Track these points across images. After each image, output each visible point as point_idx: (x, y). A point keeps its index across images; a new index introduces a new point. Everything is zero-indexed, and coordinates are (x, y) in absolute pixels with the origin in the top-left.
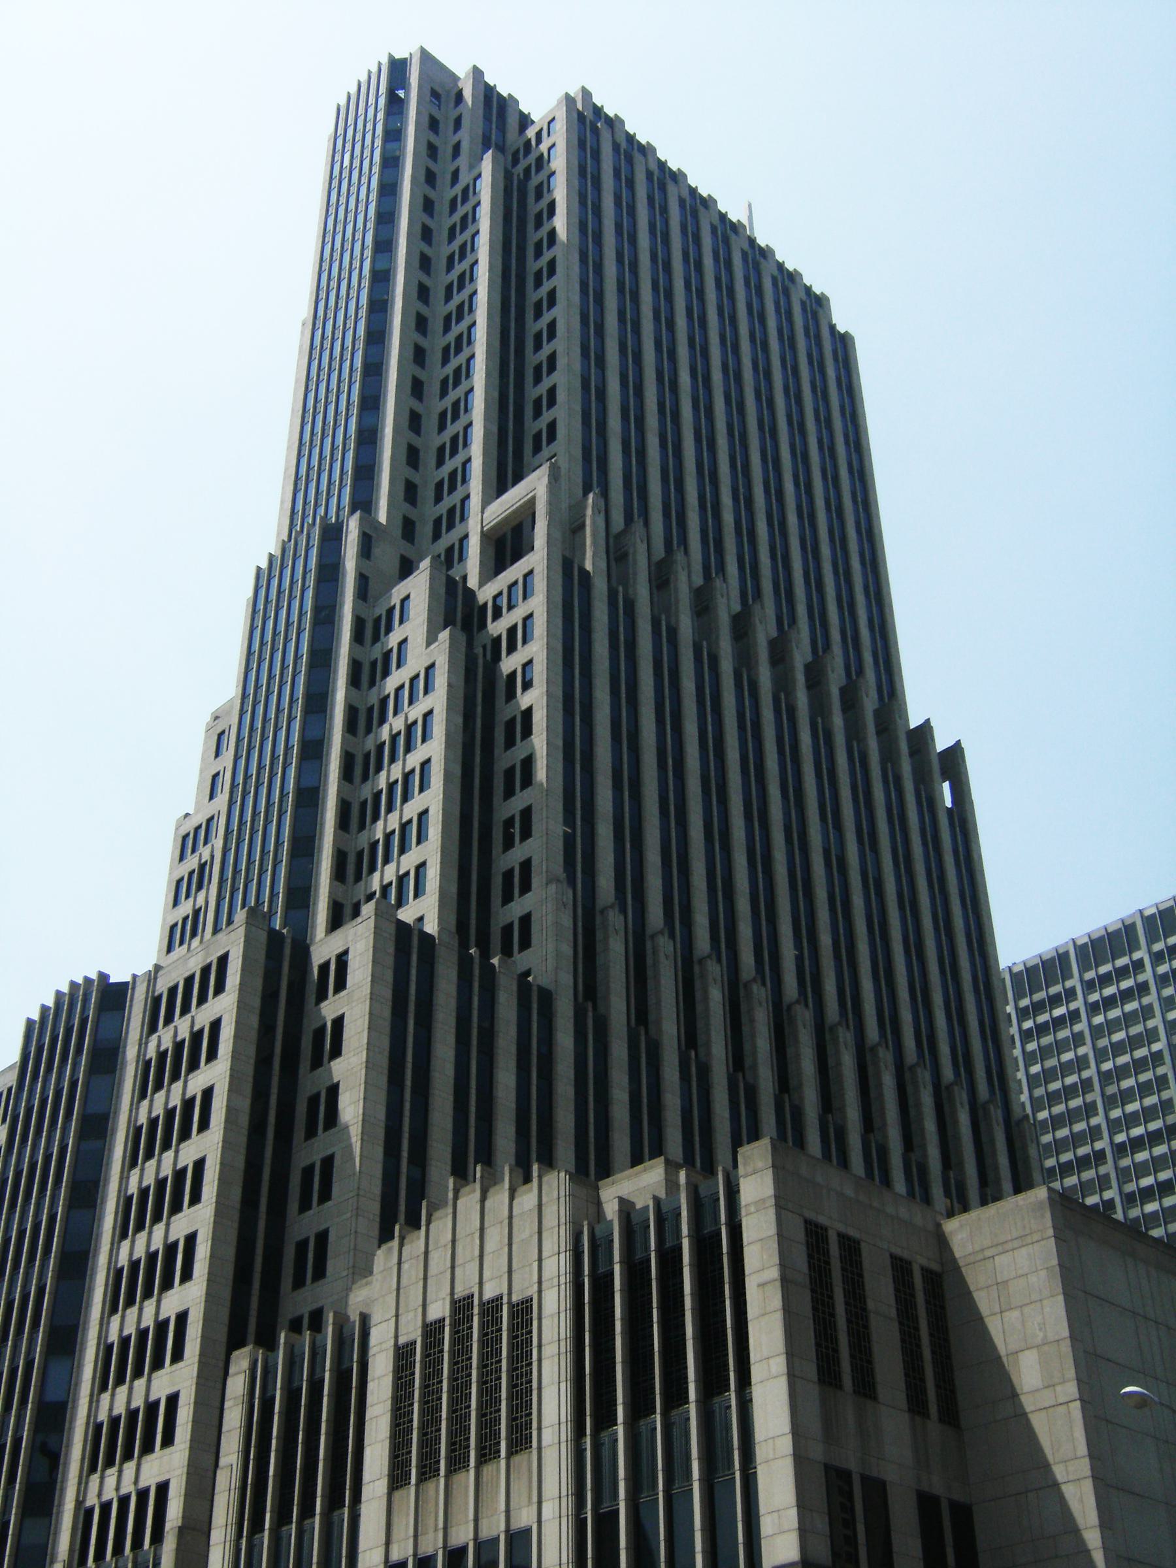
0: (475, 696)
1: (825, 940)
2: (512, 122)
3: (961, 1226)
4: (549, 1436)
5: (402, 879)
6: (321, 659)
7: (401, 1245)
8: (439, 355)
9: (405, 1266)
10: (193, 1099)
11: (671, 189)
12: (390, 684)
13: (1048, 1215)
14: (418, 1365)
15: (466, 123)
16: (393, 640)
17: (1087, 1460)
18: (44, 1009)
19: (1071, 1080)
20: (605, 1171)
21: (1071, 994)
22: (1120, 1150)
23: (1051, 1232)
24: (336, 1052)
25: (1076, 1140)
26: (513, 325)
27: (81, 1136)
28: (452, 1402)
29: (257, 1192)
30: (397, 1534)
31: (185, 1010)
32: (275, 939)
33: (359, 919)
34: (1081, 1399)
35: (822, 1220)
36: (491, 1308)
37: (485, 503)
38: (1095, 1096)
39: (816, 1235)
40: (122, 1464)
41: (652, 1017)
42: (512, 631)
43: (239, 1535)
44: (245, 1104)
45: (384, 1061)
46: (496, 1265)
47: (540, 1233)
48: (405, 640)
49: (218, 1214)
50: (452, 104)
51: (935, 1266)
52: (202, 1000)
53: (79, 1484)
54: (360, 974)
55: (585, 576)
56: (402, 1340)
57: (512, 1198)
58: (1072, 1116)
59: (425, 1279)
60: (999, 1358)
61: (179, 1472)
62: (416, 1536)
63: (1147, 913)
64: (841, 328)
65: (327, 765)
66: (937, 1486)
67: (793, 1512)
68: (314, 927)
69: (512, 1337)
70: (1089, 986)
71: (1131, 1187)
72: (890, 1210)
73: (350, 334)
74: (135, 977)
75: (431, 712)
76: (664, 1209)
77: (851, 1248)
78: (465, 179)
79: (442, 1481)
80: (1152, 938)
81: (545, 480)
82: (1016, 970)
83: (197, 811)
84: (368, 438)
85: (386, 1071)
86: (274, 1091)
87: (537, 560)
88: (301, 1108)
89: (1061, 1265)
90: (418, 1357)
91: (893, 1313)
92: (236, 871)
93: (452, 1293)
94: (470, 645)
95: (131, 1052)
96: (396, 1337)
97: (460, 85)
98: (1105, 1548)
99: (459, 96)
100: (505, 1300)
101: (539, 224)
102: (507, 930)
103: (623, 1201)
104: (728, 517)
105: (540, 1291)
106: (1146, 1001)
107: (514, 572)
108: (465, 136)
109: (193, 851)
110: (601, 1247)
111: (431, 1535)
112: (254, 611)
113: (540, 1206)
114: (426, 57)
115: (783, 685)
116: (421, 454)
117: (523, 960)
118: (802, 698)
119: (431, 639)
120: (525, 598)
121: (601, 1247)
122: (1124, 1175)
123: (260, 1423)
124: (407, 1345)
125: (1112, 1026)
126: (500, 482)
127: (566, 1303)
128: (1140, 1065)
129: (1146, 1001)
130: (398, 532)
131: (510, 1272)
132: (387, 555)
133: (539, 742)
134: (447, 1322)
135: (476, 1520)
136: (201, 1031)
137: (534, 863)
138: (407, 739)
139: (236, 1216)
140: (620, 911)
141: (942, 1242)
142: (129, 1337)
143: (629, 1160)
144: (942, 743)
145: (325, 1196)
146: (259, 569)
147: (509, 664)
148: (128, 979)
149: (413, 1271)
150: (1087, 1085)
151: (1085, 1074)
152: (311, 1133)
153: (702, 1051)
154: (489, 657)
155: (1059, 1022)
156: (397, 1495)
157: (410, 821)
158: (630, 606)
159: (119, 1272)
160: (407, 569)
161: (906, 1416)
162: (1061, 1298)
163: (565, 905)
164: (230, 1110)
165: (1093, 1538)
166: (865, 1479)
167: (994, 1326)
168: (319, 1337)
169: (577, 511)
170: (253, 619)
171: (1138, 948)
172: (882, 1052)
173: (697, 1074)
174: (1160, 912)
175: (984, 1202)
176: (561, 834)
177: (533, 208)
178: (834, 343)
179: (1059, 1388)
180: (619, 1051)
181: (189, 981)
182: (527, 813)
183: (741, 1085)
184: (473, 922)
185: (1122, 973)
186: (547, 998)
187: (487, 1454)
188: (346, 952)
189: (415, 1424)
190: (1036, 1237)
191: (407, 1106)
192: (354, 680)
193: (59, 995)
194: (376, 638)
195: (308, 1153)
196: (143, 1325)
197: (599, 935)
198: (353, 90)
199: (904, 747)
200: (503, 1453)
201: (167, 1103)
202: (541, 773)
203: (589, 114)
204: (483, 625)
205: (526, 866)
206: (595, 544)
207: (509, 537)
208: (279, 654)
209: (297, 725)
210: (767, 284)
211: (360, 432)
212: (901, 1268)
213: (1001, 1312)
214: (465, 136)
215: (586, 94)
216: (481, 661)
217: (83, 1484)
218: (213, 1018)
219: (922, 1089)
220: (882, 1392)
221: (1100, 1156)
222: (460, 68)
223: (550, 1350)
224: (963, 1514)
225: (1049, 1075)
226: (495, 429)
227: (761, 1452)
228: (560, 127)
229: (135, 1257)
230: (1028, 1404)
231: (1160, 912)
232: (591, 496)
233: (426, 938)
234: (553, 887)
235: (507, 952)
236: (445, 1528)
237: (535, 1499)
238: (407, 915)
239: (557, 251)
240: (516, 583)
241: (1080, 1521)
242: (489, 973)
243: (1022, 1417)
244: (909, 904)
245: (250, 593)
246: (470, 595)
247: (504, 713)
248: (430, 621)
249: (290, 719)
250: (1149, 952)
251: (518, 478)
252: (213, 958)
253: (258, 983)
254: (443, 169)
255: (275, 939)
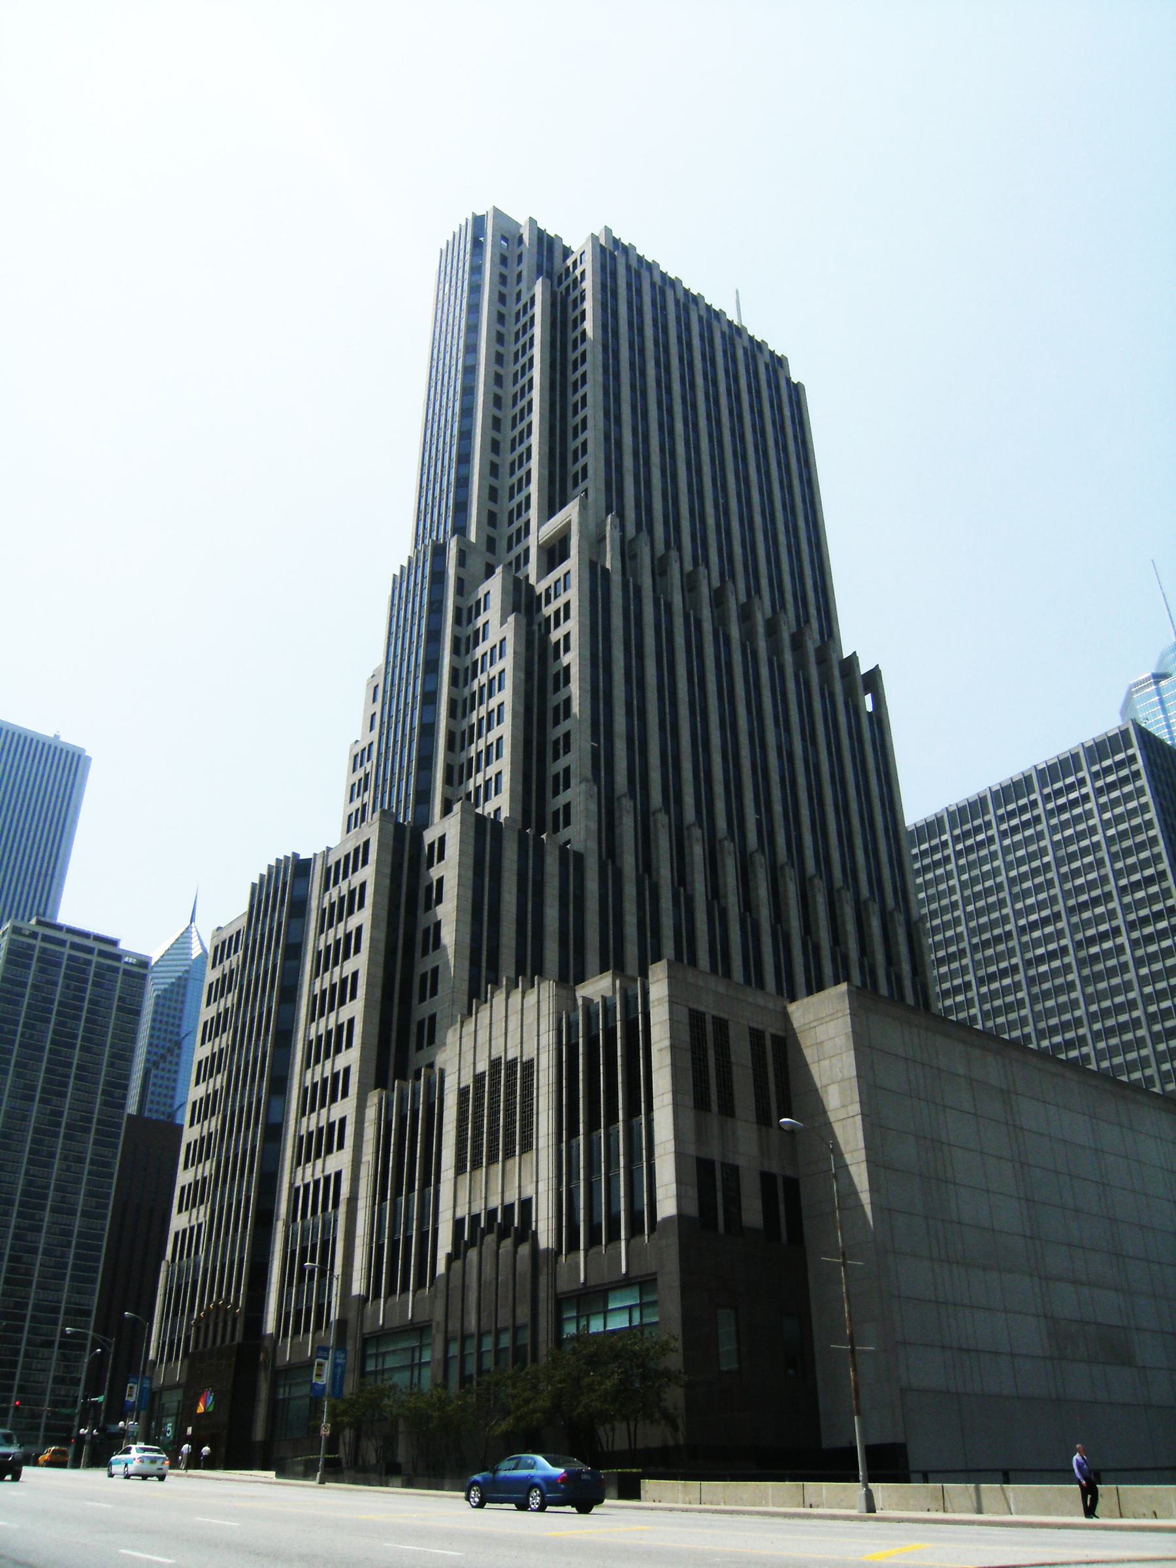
0: (533, 657)
1: (778, 808)
2: (558, 254)
3: (797, 1008)
4: (543, 1142)
5: (487, 783)
6: (434, 636)
7: (462, 1027)
8: (510, 422)
9: (464, 1040)
10: (351, 933)
11: (670, 294)
12: (479, 652)
13: (847, 1001)
14: (471, 1100)
15: (525, 259)
16: (480, 622)
17: (864, 1151)
18: (262, 876)
19: (988, 884)
20: (581, 978)
21: (988, 825)
22: (1022, 930)
23: (848, 1011)
24: (439, 900)
25: (993, 924)
26: (558, 399)
27: (286, 957)
28: (490, 1122)
29: (392, 991)
30: (459, 1201)
31: (345, 876)
32: (399, 828)
33: (452, 814)
34: (862, 1114)
35: (701, 1008)
36: (512, 1064)
37: (540, 525)
38: (1005, 894)
39: (697, 1018)
40: (315, 1161)
41: (654, 867)
42: (557, 613)
43: (374, 1204)
44: (382, 936)
45: (468, 905)
46: (514, 1039)
47: (538, 1019)
48: (487, 622)
49: (366, 1006)
50: (516, 244)
51: (780, 1033)
52: (355, 870)
53: (291, 1173)
54: (452, 850)
55: (605, 572)
56: (462, 1085)
57: (523, 997)
58: (989, 908)
59: (475, 1048)
60: (817, 1090)
61: (346, 1165)
62: (470, 1203)
63: (1040, 767)
64: (795, 380)
65: (439, 707)
66: (775, 1167)
67: (674, 1186)
68: (433, 816)
69: (523, 1083)
70: (1001, 819)
71: (1029, 955)
72: (750, 999)
73: (450, 411)
74: (315, 855)
75: (503, 671)
76: (608, 1003)
77: (721, 1025)
78: (525, 298)
79: (484, 1169)
80: (1043, 785)
81: (577, 508)
82: (951, 809)
83: (363, 739)
84: (463, 483)
85: (470, 912)
86: (401, 926)
87: (572, 564)
88: (419, 936)
89: (854, 1032)
90: (471, 1096)
91: (750, 1064)
92: (384, 780)
93: (490, 1056)
94: (530, 624)
95: (314, 903)
96: (459, 1083)
97: (521, 231)
98: (872, 1203)
99: (520, 240)
100: (519, 1060)
101: (575, 327)
102: (556, 814)
103: (584, 998)
104: (711, 521)
105: (538, 1054)
106: (1039, 828)
107: (558, 572)
108: (524, 267)
109: (361, 766)
110: (572, 1027)
111: (478, 1202)
112: (392, 604)
113: (539, 1002)
114: (497, 213)
115: (748, 636)
116: (499, 492)
117: (564, 834)
118: (762, 645)
119: (503, 621)
120: (565, 590)
121: (572, 1027)
122: (1024, 947)
123: (568, 1105)
124: (463, 1089)
125: (1016, 846)
126: (552, 507)
127: (553, 1062)
128: (1035, 872)
129: (1039, 828)
130: (484, 548)
131: (522, 1043)
132: (476, 564)
133: (574, 688)
134: (487, 1074)
135: (503, 1192)
136: (355, 889)
137: (572, 768)
138: (489, 689)
139: (378, 1007)
140: (631, 798)
141: (786, 1017)
142: (317, 1083)
143: (598, 968)
144: (864, 668)
145: (434, 992)
146: (402, 567)
147: (556, 635)
148: (311, 856)
149: (468, 1042)
150: (999, 887)
151: (998, 880)
152: (425, 952)
153: (689, 887)
154: (543, 631)
155: (980, 845)
156: (460, 1178)
157: (492, 744)
158: (638, 590)
159: (311, 1042)
160: (489, 572)
161: (755, 1126)
162: (852, 1052)
163: (591, 796)
164: (372, 939)
165: (865, 1198)
166: (723, 1164)
167: (814, 1070)
168: (417, 1083)
169: (601, 526)
170: (392, 610)
171: (1034, 792)
172: (817, 881)
173: (685, 902)
174: (1048, 767)
175: (810, 993)
176: (589, 748)
177: (572, 315)
178: (789, 390)
179: (849, 1107)
180: (630, 890)
181: (347, 857)
182: (567, 735)
183: (716, 908)
184: (534, 808)
185: (1023, 810)
186: (579, 858)
187: (509, 1154)
188: (444, 836)
189: (469, 1135)
190: (840, 1014)
191: (485, 934)
192: (456, 650)
193: (270, 867)
194: (469, 621)
195: (424, 966)
196: (325, 1076)
197: (617, 814)
198: (450, 239)
199: (836, 672)
200: (517, 1153)
201: (335, 936)
202: (575, 708)
203: (610, 247)
204: (539, 609)
205: (567, 770)
206: (612, 549)
207: (557, 547)
208: (416, 627)
209: (419, 681)
210: (740, 353)
211: (458, 480)
212: (757, 1036)
213: (819, 1061)
214: (524, 267)
215: (608, 231)
216: (537, 636)
217: (293, 1173)
218: (361, 882)
219: (845, 904)
220: (739, 1112)
221: (1008, 935)
222: (521, 219)
223: (544, 1090)
224: (793, 1185)
225: (974, 881)
226: (546, 472)
227: (658, 1151)
228: (588, 257)
229: (329, 1028)
230: (832, 1117)
231: (1048, 767)
232: (610, 516)
233: (495, 822)
234: (583, 786)
235: (556, 830)
236: (486, 1198)
237: (535, 1179)
238: (488, 809)
239: (587, 346)
240: (559, 580)
241: (859, 1188)
242: (540, 846)
243: (828, 1124)
244: (839, 781)
245: (390, 593)
246: (531, 588)
247: (553, 669)
248: (503, 609)
249: (415, 678)
250: (1041, 794)
251: (563, 504)
252: (361, 842)
253: (389, 858)
254: (511, 290)
255: (399, 828)
